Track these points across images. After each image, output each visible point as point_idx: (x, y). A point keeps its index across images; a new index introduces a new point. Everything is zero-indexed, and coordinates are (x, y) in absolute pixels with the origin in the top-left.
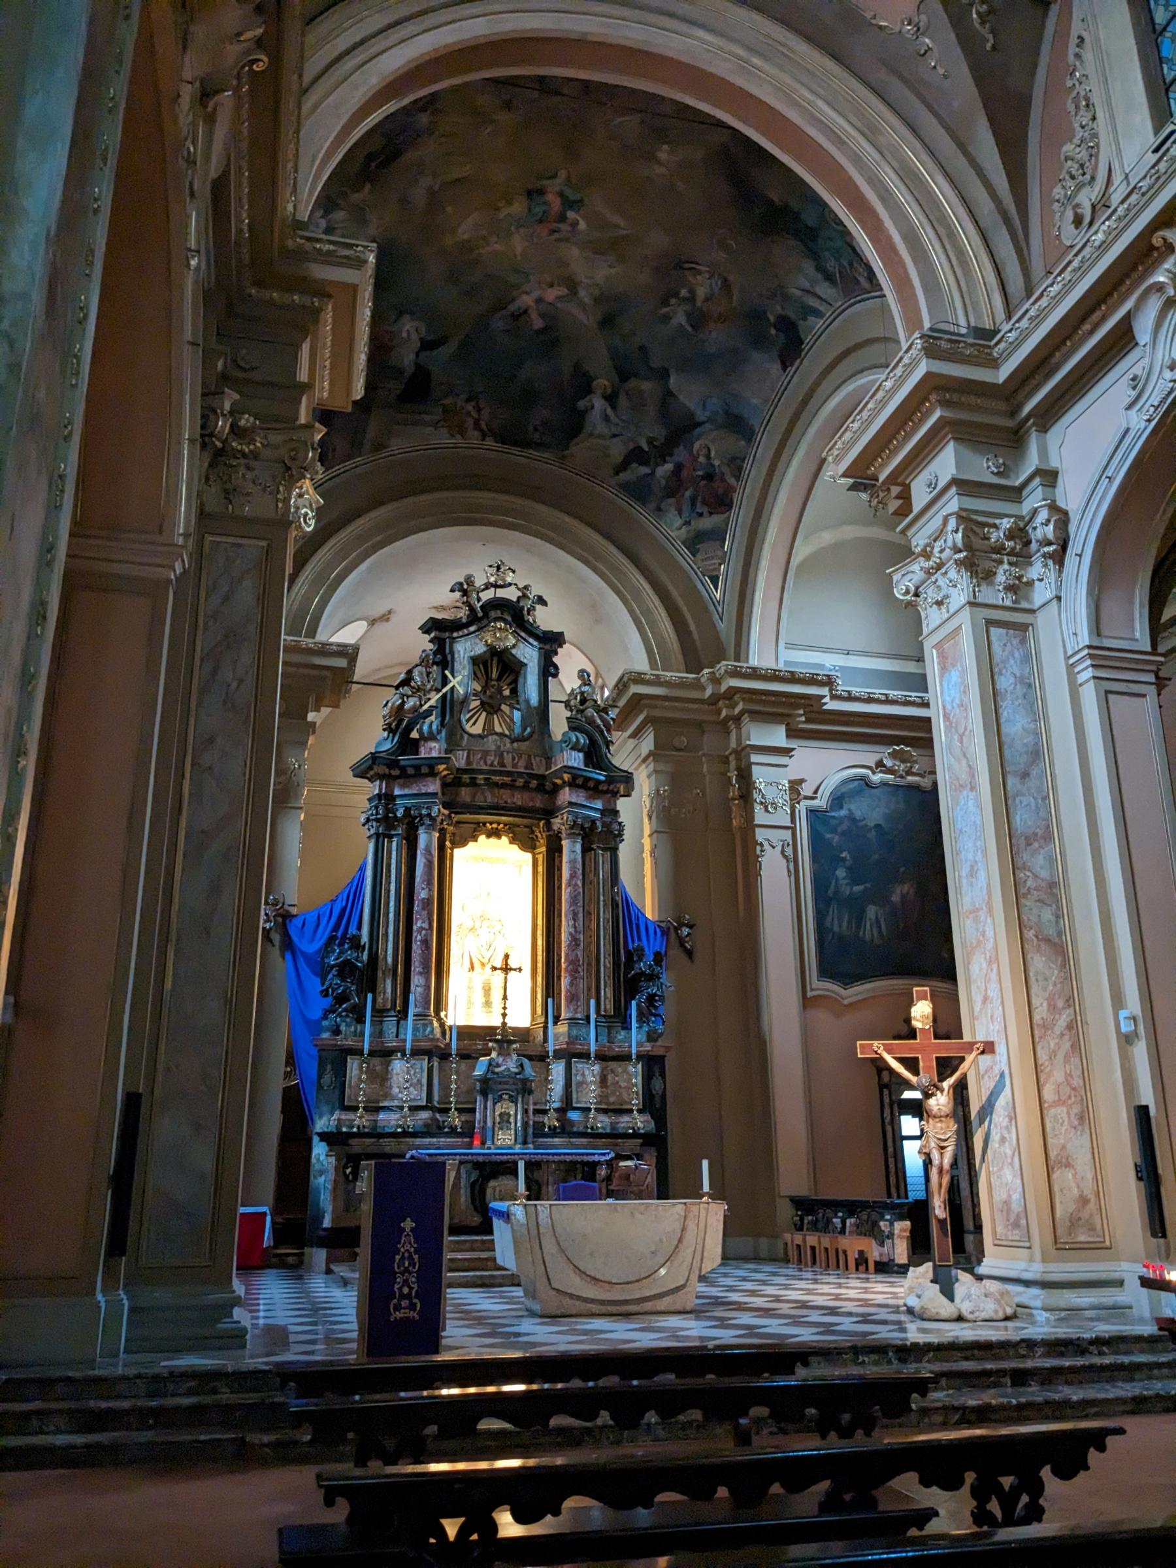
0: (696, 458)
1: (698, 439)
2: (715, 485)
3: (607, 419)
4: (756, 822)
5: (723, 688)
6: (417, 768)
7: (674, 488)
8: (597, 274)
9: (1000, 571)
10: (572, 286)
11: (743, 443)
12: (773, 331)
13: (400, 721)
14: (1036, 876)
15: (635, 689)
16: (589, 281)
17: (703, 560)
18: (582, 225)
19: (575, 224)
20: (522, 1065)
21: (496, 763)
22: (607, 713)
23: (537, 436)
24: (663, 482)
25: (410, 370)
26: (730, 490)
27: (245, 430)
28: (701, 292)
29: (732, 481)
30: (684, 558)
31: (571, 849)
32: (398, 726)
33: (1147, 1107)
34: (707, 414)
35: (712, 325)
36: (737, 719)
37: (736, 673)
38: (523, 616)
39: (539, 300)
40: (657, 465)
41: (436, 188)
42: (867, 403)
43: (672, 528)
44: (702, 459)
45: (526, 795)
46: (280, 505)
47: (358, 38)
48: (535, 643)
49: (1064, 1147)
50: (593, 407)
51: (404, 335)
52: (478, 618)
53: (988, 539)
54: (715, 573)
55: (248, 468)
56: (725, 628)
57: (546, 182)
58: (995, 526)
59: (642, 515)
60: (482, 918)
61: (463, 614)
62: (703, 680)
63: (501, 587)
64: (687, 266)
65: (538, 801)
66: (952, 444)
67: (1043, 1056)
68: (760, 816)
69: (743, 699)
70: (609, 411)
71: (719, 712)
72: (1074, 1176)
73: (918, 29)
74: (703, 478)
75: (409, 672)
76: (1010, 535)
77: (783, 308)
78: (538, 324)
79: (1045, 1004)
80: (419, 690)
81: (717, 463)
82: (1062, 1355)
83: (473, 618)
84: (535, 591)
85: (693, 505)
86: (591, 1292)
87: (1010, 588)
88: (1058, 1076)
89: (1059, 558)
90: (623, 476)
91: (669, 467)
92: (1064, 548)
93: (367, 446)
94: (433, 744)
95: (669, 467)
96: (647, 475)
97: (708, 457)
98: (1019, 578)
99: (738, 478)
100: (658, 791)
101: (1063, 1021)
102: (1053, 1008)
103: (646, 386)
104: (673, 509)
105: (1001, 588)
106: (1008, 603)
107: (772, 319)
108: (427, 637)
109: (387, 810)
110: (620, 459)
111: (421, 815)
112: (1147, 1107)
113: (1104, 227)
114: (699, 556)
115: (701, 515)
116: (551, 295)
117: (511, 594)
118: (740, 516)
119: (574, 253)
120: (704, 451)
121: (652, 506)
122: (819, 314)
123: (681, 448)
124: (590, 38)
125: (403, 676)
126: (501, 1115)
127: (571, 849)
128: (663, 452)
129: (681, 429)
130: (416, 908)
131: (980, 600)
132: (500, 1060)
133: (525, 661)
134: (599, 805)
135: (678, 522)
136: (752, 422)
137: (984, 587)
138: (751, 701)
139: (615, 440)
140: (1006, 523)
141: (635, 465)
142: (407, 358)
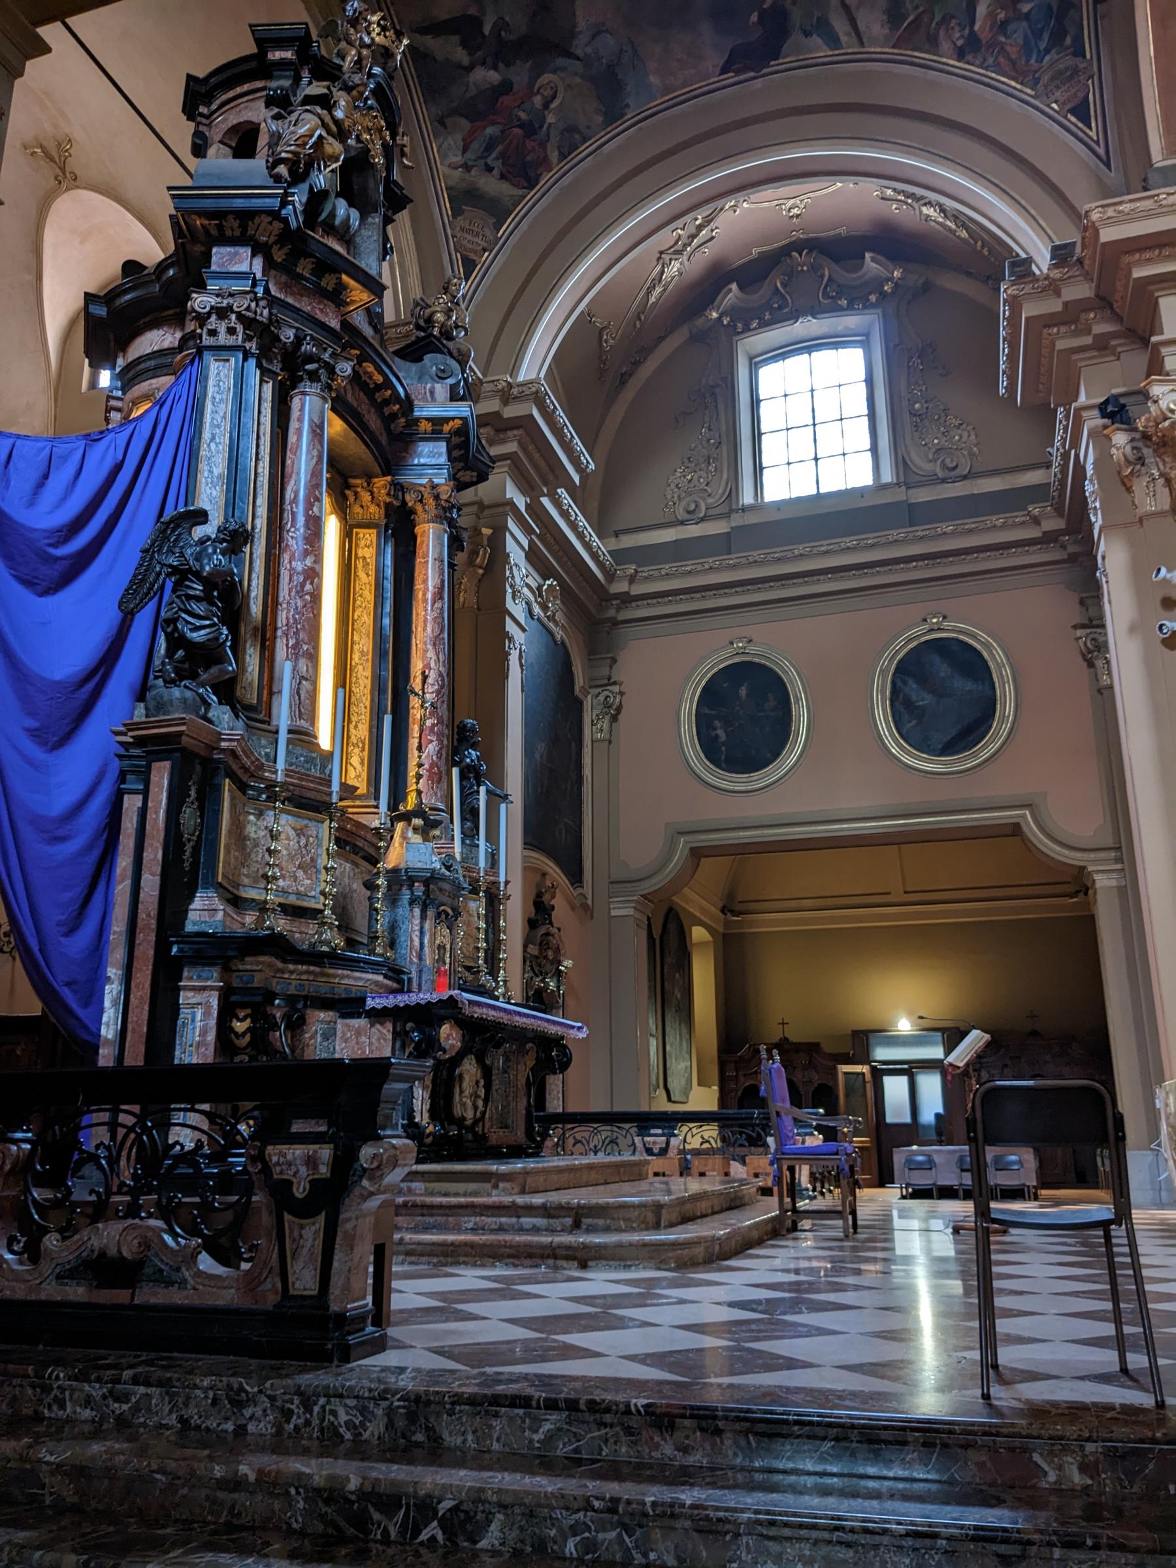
0: (531, 93)
1: (554, 72)
2: (529, 144)
7: (481, 108)
11: (600, 119)
12: (754, 18)
24: (473, 92)
26: (545, 163)
29: (554, 156)
33: (699, 1084)
34: (589, 50)
44: (538, 100)
74: (522, 126)
81: (551, 119)
85: (489, 148)
90: (431, 43)
91: (494, 77)
95: (494, 77)
96: (460, 66)
97: (546, 106)
99: (563, 157)
104: (459, 137)
110: (442, 14)
112: (699, 1084)
115: (490, 169)
118: (535, 211)
120: (548, 93)
122: (833, 41)
128: (503, 52)
135: (457, 159)
136: (630, 101)
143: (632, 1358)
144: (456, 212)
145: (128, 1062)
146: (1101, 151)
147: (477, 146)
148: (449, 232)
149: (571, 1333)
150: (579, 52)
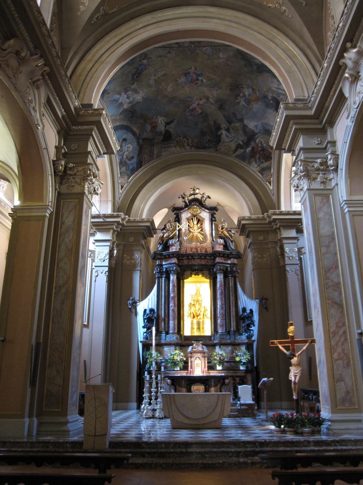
1: (257, 138)
2: (265, 152)
3: (228, 136)
4: (286, 263)
5: (272, 219)
6: (169, 255)
7: (253, 154)
8: (214, 94)
9: (319, 177)
10: (207, 98)
13: (163, 241)
14: (332, 281)
15: (243, 222)
16: (212, 96)
17: (265, 177)
18: (204, 81)
19: (202, 81)
20: (203, 348)
21: (195, 251)
22: (231, 232)
23: (207, 145)
25: (164, 132)
27: (72, 167)
28: (247, 93)
30: (259, 176)
31: (220, 278)
32: (162, 242)
34: (258, 130)
35: (253, 103)
36: (279, 228)
37: (275, 214)
38: (202, 203)
39: (198, 105)
40: (246, 148)
41: (157, 79)
42: (275, 127)
43: (254, 169)
44: (260, 145)
45: (205, 261)
46: (82, 188)
47: (108, 47)
48: (208, 211)
49: (341, 374)
50: (222, 133)
51: (160, 122)
52: (188, 206)
53: (314, 167)
54: (269, 181)
55: (73, 178)
56: (274, 198)
57: (189, 70)
58: (316, 162)
59: (244, 164)
60: (197, 301)
61: (183, 205)
62: (265, 217)
63: (196, 194)
64: (240, 86)
65: (210, 263)
66: (301, 136)
67: (333, 343)
68: (287, 261)
69: (279, 222)
70: (228, 134)
71: (273, 227)
72: (345, 384)
73: (280, 5)
74: (261, 151)
75: (165, 225)
76: (321, 164)
77: (272, 95)
78: (200, 111)
79: (335, 326)
80: (168, 231)
81: (264, 145)
82: (320, 446)
83: (186, 206)
84: (207, 194)
86: (186, 421)
87: (323, 183)
88: (340, 350)
89: (336, 170)
90: (238, 153)
91: (250, 148)
92: (337, 167)
93: (155, 156)
94: (173, 247)
95: (250, 148)
96: (244, 152)
98: (326, 179)
100: (254, 255)
101: (341, 332)
102: (337, 326)
103: (237, 125)
105: (319, 183)
106: (322, 188)
107: (270, 98)
108: (174, 213)
109: (160, 269)
110: (234, 148)
111: (170, 270)
113: (326, 62)
114: (264, 176)
115: (263, 162)
116: (201, 102)
117: (199, 197)
119: (205, 89)
121: (247, 161)
123: (252, 142)
124: (180, 30)
125: (163, 227)
126: (197, 364)
127: (220, 278)
128: (247, 144)
129: (251, 137)
130: (170, 300)
131: (312, 187)
132: (196, 346)
133: (204, 217)
134: (229, 262)
135: (256, 166)
137: (313, 182)
138: (282, 222)
139: (231, 143)
140: (319, 161)
141: (239, 149)
142: (161, 127)
143: (132, 438)
144: (262, 175)
145: (109, 245)
146: (120, 196)
147: (258, 160)
148: (263, 179)
149: (43, 20)
150: (257, 132)
